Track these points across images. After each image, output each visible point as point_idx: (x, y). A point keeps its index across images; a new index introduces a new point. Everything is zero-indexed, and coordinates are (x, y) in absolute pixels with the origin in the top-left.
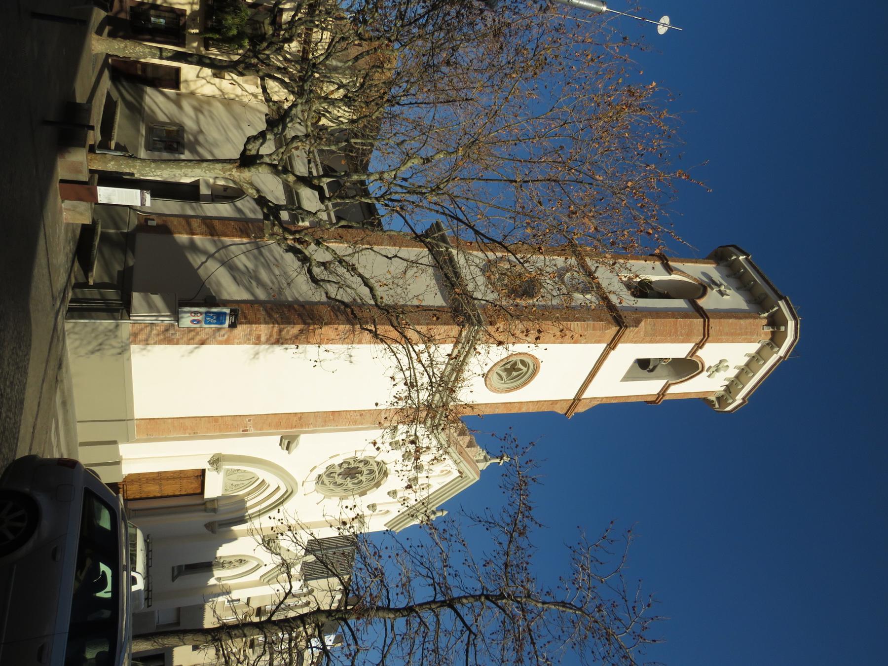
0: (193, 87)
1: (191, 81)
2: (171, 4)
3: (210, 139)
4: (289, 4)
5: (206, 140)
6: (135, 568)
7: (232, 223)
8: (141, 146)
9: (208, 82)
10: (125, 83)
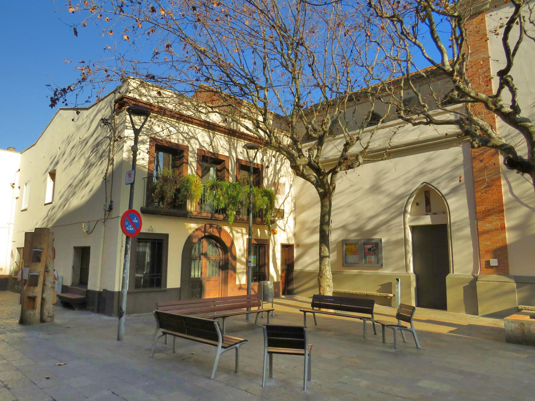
0: (291, 235)
1: (287, 236)
2: (245, 251)
3: (352, 219)
4: (232, 153)
5: (355, 223)
6: (508, 270)
7: (478, 195)
8: (376, 273)
9: (287, 223)
10: (295, 286)
